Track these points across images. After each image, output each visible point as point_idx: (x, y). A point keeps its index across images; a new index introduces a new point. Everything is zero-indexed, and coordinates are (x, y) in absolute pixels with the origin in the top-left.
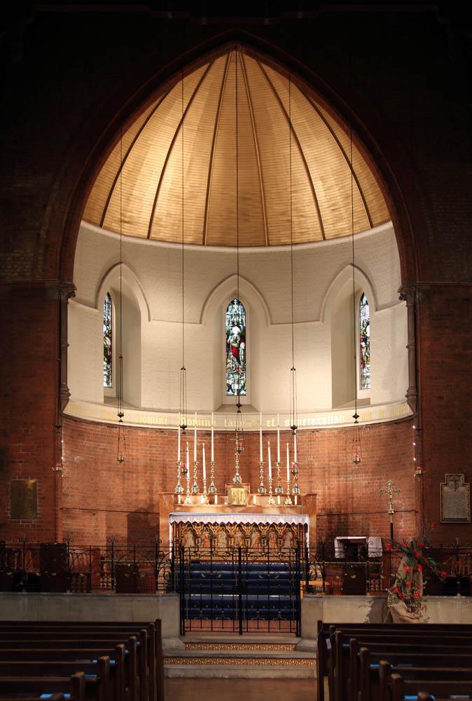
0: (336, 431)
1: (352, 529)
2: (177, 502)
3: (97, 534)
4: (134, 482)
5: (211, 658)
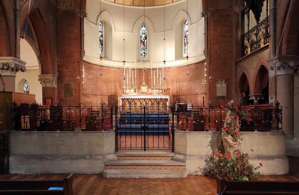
0: (176, 68)
1: (181, 101)
2: (124, 92)
3: (97, 103)
4: (110, 85)
5: (130, 165)
